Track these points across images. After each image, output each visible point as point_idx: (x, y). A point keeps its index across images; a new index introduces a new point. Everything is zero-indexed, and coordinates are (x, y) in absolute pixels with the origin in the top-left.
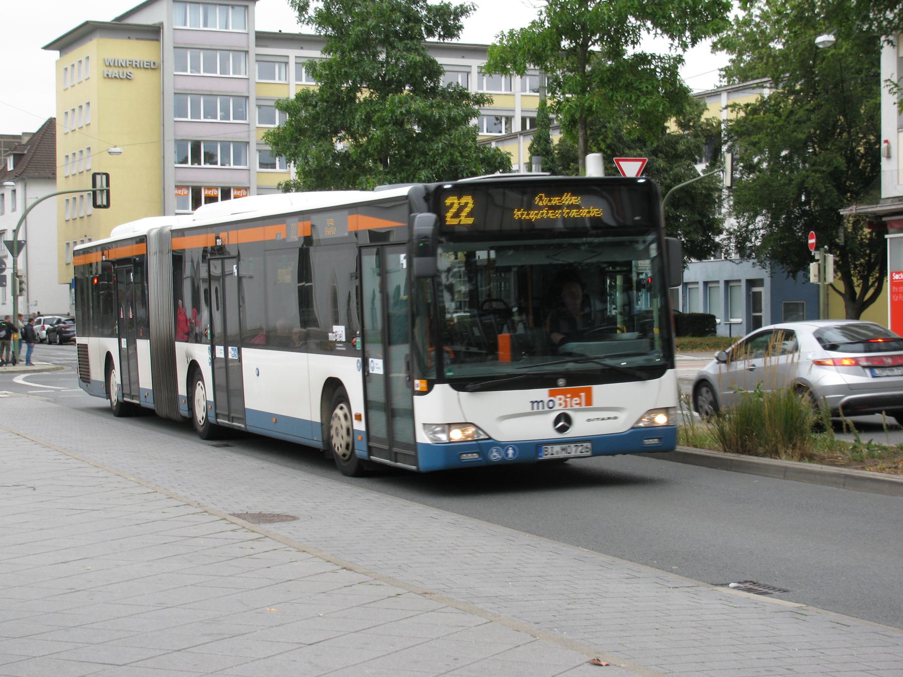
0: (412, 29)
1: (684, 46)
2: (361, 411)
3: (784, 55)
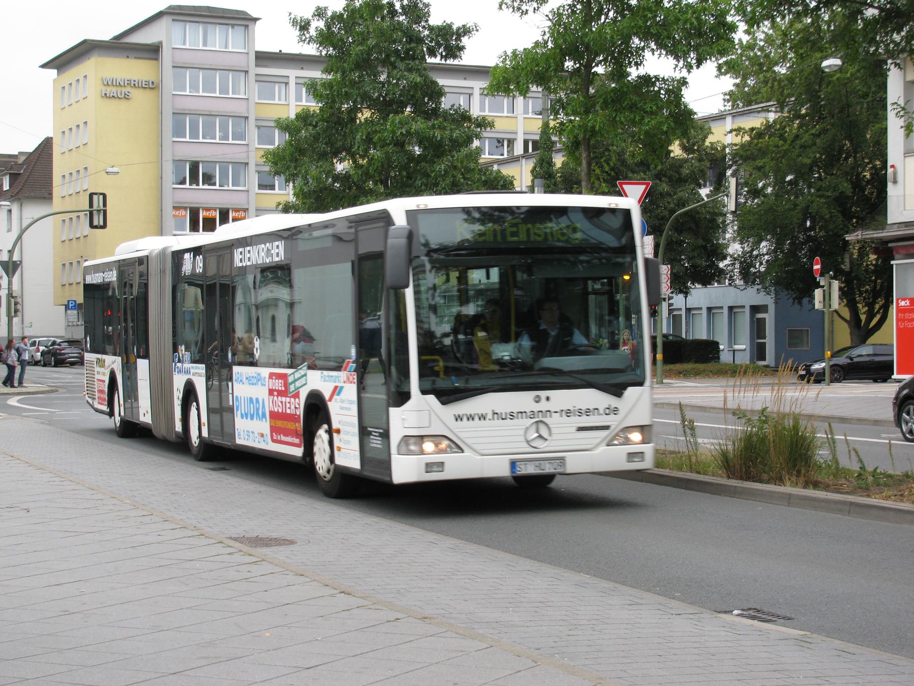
1: (689, 68)
3: (790, 79)
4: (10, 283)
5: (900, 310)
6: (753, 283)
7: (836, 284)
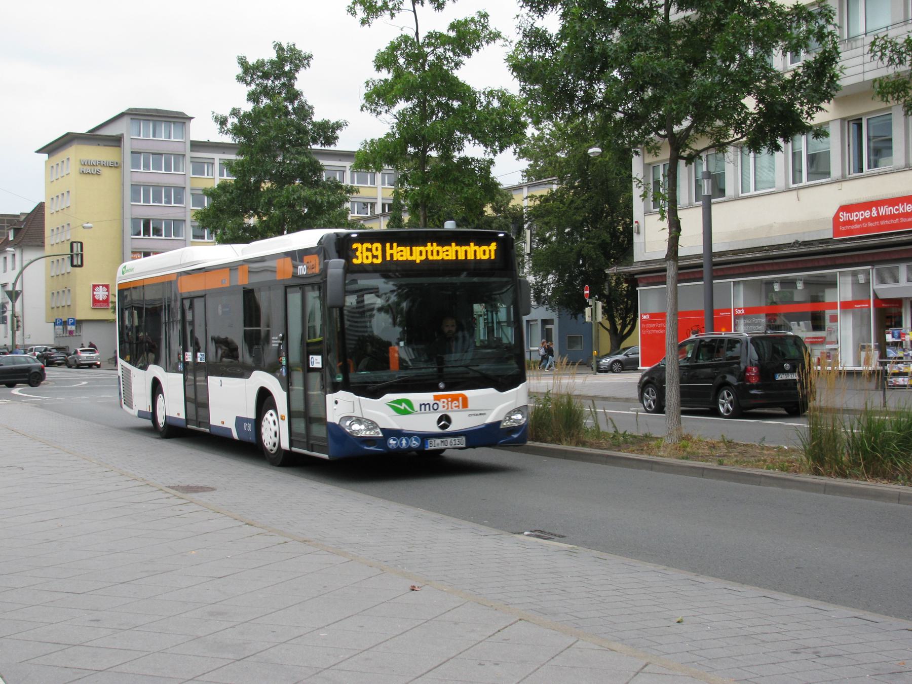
1: (495, 153)
3: (567, 161)
4: (13, 306)
5: (643, 322)
6: (544, 303)
7: (600, 304)
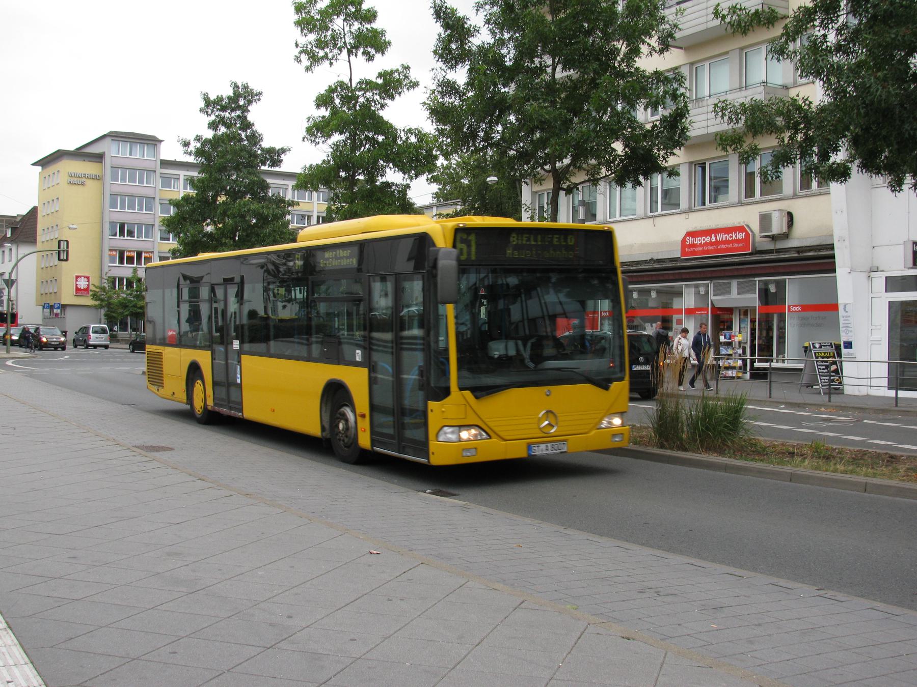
0: (252, 161)
1: (411, 178)
2: (367, 412)
3: (469, 187)
4: (9, 292)
